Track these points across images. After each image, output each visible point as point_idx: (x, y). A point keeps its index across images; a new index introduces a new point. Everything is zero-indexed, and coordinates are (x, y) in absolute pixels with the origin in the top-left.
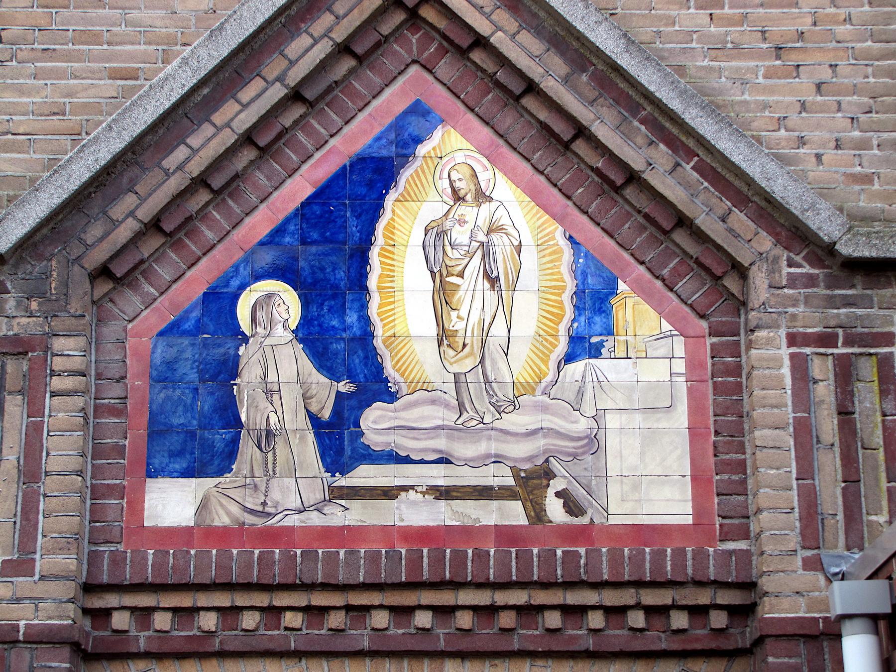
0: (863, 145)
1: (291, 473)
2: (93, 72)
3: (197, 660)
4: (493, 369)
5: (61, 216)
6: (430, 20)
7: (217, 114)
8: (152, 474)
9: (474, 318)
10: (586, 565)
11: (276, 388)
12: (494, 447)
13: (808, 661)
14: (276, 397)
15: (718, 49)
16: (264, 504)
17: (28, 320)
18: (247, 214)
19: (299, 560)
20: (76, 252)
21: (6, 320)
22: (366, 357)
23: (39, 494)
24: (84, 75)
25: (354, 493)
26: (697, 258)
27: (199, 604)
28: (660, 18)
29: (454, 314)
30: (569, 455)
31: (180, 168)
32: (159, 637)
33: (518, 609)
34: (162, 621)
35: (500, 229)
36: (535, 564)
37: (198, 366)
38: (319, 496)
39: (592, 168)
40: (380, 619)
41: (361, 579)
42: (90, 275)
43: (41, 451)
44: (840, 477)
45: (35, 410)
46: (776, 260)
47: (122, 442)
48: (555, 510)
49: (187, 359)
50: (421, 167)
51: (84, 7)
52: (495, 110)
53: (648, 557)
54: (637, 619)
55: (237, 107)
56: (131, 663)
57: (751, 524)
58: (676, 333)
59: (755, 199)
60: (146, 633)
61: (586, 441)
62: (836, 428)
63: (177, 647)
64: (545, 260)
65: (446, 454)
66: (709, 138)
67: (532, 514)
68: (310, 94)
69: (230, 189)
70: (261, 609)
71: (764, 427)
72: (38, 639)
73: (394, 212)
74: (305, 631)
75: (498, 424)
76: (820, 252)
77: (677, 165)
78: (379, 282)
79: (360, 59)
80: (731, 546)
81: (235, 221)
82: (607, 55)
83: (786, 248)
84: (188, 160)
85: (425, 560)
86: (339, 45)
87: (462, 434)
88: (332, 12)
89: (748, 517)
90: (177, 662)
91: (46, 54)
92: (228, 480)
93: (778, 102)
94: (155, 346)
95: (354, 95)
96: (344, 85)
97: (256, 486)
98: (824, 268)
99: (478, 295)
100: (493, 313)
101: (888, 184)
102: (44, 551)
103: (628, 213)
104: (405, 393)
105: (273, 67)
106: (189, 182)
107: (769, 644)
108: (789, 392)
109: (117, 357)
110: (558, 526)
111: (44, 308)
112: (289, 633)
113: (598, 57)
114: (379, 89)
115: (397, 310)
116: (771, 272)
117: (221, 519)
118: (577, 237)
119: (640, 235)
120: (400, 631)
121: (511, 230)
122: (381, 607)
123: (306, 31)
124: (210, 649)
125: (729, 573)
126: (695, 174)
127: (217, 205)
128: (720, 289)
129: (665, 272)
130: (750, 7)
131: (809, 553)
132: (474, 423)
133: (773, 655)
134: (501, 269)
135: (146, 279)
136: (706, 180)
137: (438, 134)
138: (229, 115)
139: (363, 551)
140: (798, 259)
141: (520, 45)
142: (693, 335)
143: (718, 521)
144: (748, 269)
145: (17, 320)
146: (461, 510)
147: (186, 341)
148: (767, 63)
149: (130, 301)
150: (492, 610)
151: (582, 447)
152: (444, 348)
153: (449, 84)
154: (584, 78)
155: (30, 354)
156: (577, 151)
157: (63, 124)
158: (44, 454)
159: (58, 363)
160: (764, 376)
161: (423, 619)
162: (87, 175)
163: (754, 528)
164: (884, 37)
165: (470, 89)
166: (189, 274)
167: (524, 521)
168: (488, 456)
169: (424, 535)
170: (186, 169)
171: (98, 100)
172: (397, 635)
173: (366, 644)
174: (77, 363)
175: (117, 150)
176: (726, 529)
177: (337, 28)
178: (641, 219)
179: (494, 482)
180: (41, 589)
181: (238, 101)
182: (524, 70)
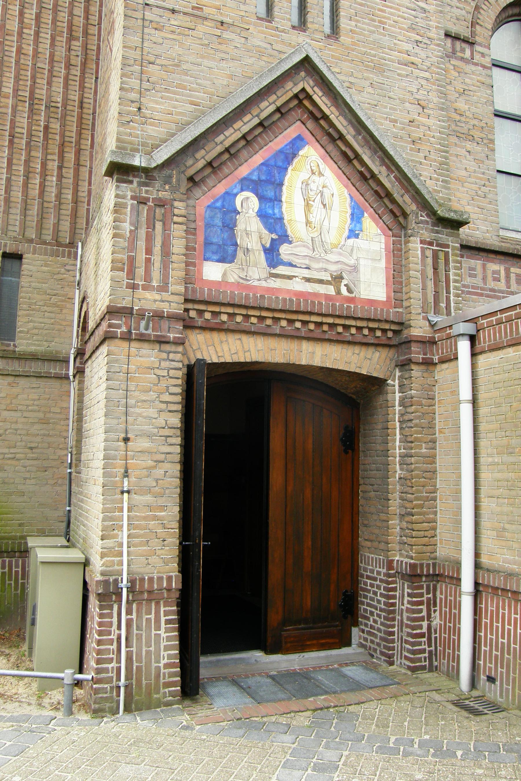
0: (437, 180)
8: (206, 259)
9: (318, 218)
11: (250, 233)
12: (324, 266)
14: (250, 236)
16: (246, 276)
18: (240, 165)
20: (183, 169)
22: (281, 226)
27: (222, 311)
30: (349, 272)
31: (221, 143)
33: (329, 324)
34: (208, 316)
35: (326, 187)
38: (265, 276)
39: (358, 171)
40: (284, 323)
43: (170, 245)
44: (433, 290)
46: (417, 214)
48: (344, 291)
54: (366, 332)
55: (242, 124)
63: (212, 326)
64: (341, 201)
68: (266, 124)
70: (243, 315)
73: (291, 174)
76: (430, 214)
77: (389, 175)
79: (282, 114)
84: (224, 140)
85: (302, 304)
88: (276, 95)
95: (278, 128)
99: (319, 209)
105: (255, 111)
106: (224, 149)
117: (231, 280)
118: (352, 195)
119: (372, 197)
120: (290, 328)
121: (330, 188)
122: (285, 319)
124: (224, 328)
129: (380, 212)
131: (424, 314)
132: (318, 256)
134: (326, 202)
137: (307, 147)
138: (240, 126)
144: (409, 215)
150: (335, 325)
152: (308, 227)
154: (360, 137)
159: (176, 211)
161: (298, 325)
163: (405, 304)
164: (443, 145)
165: (318, 133)
166: (218, 185)
168: (322, 269)
174: (183, 212)
177: (278, 101)
179: (324, 278)
181: (243, 121)
182: (341, 130)
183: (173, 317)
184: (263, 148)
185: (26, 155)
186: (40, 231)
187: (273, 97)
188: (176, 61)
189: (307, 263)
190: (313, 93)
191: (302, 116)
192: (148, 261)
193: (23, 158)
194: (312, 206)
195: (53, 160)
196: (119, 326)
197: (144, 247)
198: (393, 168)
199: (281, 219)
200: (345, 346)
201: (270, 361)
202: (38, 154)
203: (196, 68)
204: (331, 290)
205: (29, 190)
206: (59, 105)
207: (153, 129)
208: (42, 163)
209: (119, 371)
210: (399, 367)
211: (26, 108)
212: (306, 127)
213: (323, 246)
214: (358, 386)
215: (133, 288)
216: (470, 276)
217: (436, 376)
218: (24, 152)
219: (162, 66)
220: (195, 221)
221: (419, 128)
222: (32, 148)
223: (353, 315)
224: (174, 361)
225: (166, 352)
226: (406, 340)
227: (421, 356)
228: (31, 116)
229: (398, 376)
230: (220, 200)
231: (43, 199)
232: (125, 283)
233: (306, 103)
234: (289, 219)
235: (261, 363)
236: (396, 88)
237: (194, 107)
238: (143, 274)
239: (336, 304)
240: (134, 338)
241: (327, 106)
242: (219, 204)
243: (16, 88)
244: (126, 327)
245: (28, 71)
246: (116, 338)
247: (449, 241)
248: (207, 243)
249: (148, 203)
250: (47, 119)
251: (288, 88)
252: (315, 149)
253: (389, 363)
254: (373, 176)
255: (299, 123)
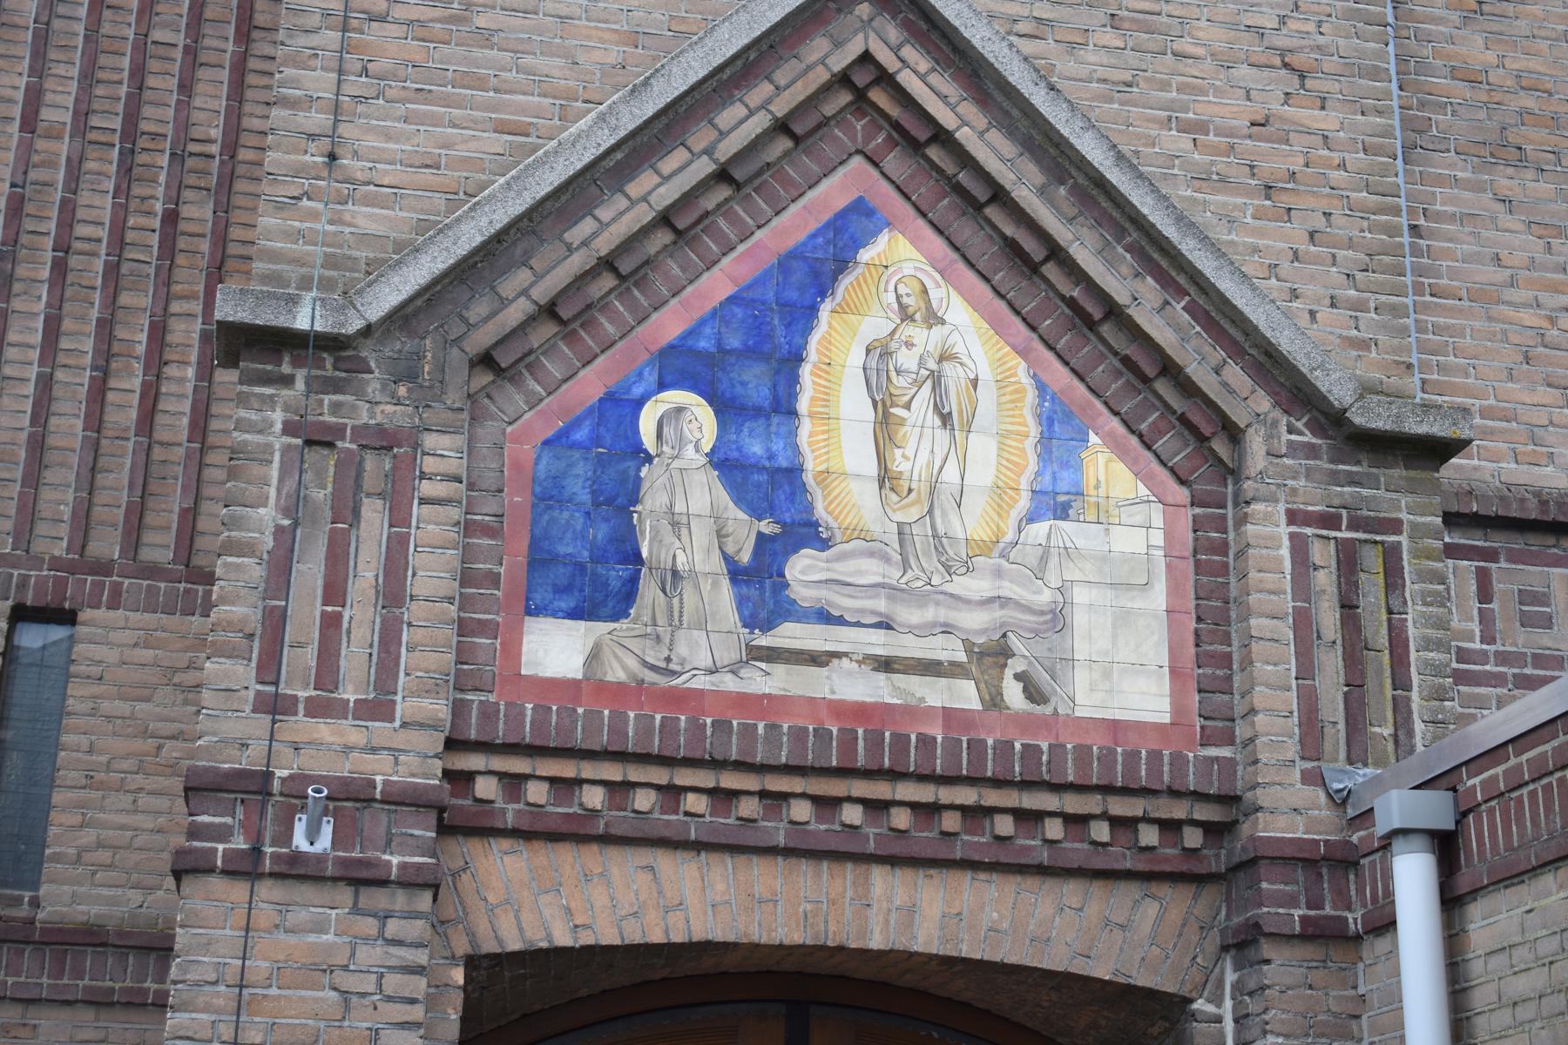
0: (1359, 307)
1: (700, 624)
2: (475, 121)
3: (574, 844)
4: (943, 522)
5: (439, 287)
6: (881, 106)
7: (632, 184)
10: (1049, 762)
11: (684, 520)
12: (943, 614)
13: (1306, 890)
14: (684, 531)
15: (1201, 178)
16: (668, 660)
17: (393, 408)
19: (709, 733)
20: (456, 330)
21: (368, 405)
23: (402, 622)
24: (465, 125)
25: (773, 655)
26: (1183, 414)
27: (584, 775)
28: (1138, 136)
29: (898, 453)
30: (1031, 631)
31: (585, 244)
32: (531, 813)
33: (963, 809)
34: (537, 792)
36: (990, 757)
37: (591, 486)
38: (735, 656)
39: (1063, 298)
40: (801, 811)
41: (784, 760)
42: (471, 361)
43: (406, 570)
44: (1342, 680)
45: (399, 517)
46: (1275, 424)
47: (496, 569)
48: (1014, 695)
49: (577, 476)
50: (863, 274)
51: (468, 45)
52: (952, 218)
53: (1120, 759)
54: (1101, 831)
55: (657, 180)
56: (492, 840)
57: (1237, 729)
58: (1154, 499)
59: (1253, 352)
60: (516, 806)
61: (1049, 617)
62: (1338, 623)
63: (552, 825)
65: (887, 617)
66: (1208, 275)
67: (987, 697)
69: (637, 277)
70: (658, 788)
71: (1261, 615)
72: (399, 800)
74: (708, 819)
75: (948, 588)
76: (1323, 420)
77: (1167, 303)
78: (811, 405)
79: (797, 139)
80: (1213, 752)
81: (641, 315)
82: (1094, 167)
83: (1285, 411)
84: (595, 235)
85: (861, 743)
86: (777, 119)
87: (905, 595)
88: (771, 82)
89: (1233, 720)
90: (549, 845)
91: (420, 96)
92: (624, 626)
93: (1268, 247)
94: (539, 458)
96: (775, 169)
97: (658, 637)
98: (1326, 438)
99: (928, 432)
100: (944, 456)
101: (1387, 353)
102: (406, 693)
103: (1102, 354)
104: (838, 540)
105: (700, 137)
107: (1263, 868)
108: (1289, 577)
109: (493, 466)
110: (1017, 713)
111: (414, 396)
112: (689, 819)
113: (1079, 169)
114: (817, 178)
115: (831, 441)
116: (1269, 437)
117: (615, 673)
119: (1116, 380)
120: (823, 827)
121: (965, 360)
122: (804, 795)
123: (740, 100)
125: (1211, 783)
126: (1186, 316)
127: (621, 294)
128: (1206, 452)
129: (1144, 427)
130: (1237, 137)
131: (1309, 765)
132: (920, 583)
133: (1267, 880)
134: (953, 405)
135: (531, 374)
136: (1199, 324)
137: (883, 239)
138: (647, 188)
139: (786, 726)
140: (1299, 425)
141: (989, 145)
142: (1172, 502)
143: (1198, 722)
144: (1243, 431)
145: (381, 407)
146: (902, 686)
147: (577, 454)
148: (1256, 202)
149: (512, 399)
151: (1045, 622)
152: (886, 491)
153: (898, 182)
154: (1062, 191)
155: (395, 450)
156: (1048, 276)
157: (438, 179)
158: (410, 573)
159: (429, 464)
160: (1261, 557)
161: (852, 814)
162: (479, 239)
163: (1241, 731)
164: (1380, 189)
165: (924, 189)
166: (582, 373)
167: (976, 705)
168: (934, 624)
169: (861, 711)
170: (593, 246)
171: (480, 155)
172: (819, 831)
173: (781, 840)
174: (454, 465)
175: (517, 213)
176: (1208, 732)
178: (1117, 364)
179: (943, 656)
180: (402, 739)
181: (658, 173)
182: (994, 174)
183: (402, 800)
184: (733, 249)
185: (104, 306)
186: (135, 535)
187: (764, 90)
188: (456, 6)
189: (883, 610)
190: (899, 65)
191: (867, 140)
192: (331, 624)
193: (95, 314)
194: (902, 422)
195: (190, 315)
196: (222, 834)
197: (320, 582)
198: (1182, 280)
199: (794, 472)
200: (1031, 882)
201: (755, 939)
202: (137, 300)
203: (519, 22)
204: (966, 695)
205: (108, 409)
206: (214, 149)
207: (372, 215)
208: (152, 325)
209: (212, 977)
210: (1233, 952)
211: (111, 163)
212: (883, 174)
213: (940, 550)
214: (1103, 1023)
215: (274, 712)
216: (1527, 621)
217: (1361, 981)
218: (97, 297)
219: (409, 23)
220: (501, 491)
221: (1287, 142)
222: (123, 282)
223: (1046, 777)
224: (399, 943)
225: (375, 916)
226: (1245, 858)
227: (1297, 913)
228: (125, 186)
229: (1232, 986)
230: (588, 423)
231: (150, 437)
232: (251, 694)
233: (878, 97)
234: (820, 468)
235: (726, 946)
236: (1203, 23)
237: (510, 138)
238: (314, 664)
239: (984, 742)
240: (267, 870)
241: (948, 104)
242: (581, 435)
243: (84, 107)
244: (247, 834)
245: (124, 55)
246: (211, 870)
247: (1400, 510)
248: (540, 559)
249: (339, 444)
250: (174, 194)
251: (814, 58)
252: (915, 241)
253: (1195, 938)
254: (1113, 311)
255: (857, 161)
